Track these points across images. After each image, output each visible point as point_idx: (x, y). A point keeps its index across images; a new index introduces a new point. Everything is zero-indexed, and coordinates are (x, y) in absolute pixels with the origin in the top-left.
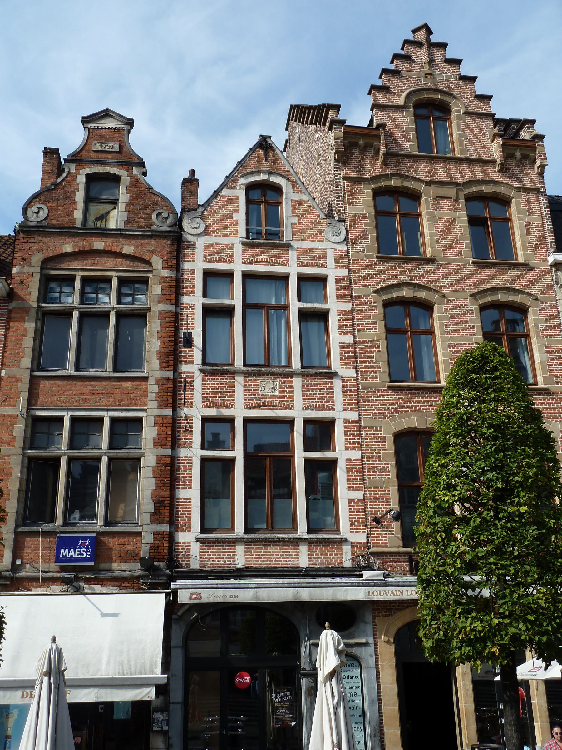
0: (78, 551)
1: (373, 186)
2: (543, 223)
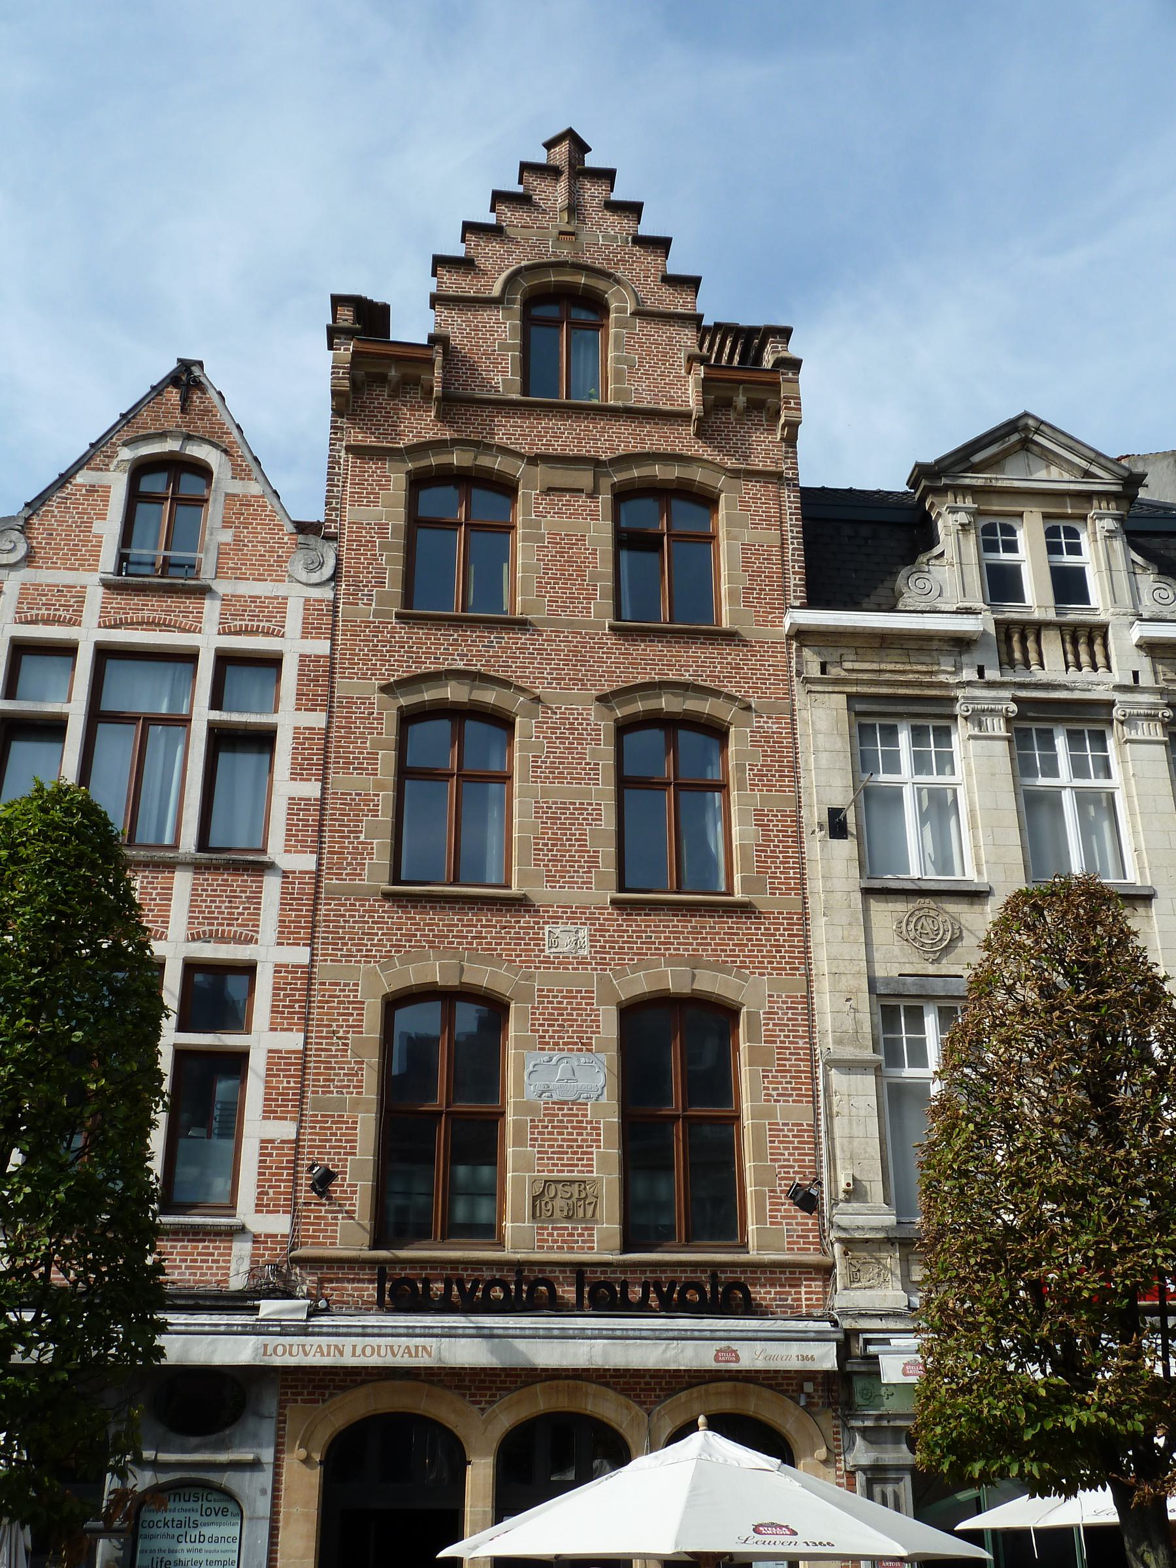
2: (783, 546)
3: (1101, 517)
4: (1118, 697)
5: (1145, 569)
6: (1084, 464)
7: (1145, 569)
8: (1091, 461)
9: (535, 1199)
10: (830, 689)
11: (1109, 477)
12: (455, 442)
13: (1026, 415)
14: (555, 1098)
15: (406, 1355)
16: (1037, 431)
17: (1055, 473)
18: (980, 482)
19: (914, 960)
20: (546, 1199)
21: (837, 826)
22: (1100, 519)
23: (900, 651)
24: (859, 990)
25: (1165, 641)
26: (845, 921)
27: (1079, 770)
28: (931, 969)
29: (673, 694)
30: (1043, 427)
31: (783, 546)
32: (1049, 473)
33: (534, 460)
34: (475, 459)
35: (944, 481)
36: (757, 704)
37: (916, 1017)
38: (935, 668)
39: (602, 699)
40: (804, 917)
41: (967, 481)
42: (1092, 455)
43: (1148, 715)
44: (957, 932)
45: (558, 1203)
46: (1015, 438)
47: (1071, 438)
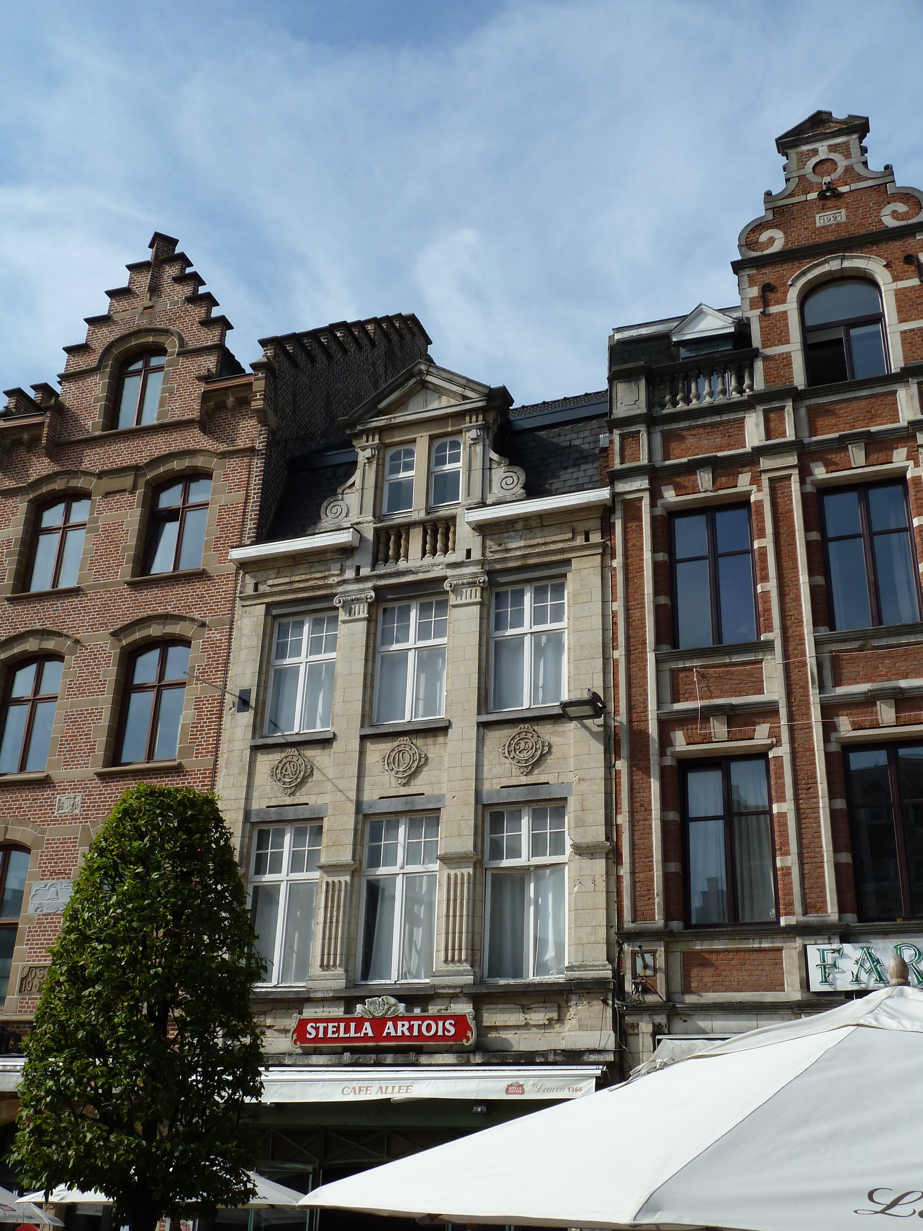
0: (334, 1027)
1: (31, 496)
2: (246, 502)
4: (449, 572)
5: (499, 463)
6: (459, 390)
9: (22, 980)
10: (255, 602)
12: (57, 474)
14: (44, 912)
17: (445, 401)
18: (383, 423)
19: (279, 795)
20: (29, 979)
21: (243, 703)
22: (469, 431)
23: (306, 565)
24: (237, 821)
26: (237, 771)
28: (289, 801)
29: (157, 623)
31: (246, 502)
33: (101, 475)
34: (68, 482)
35: (359, 428)
36: (211, 621)
38: (327, 573)
39: (113, 634)
40: (214, 771)
41: (374, 424)
42: (464, 382)
43: (469, 583)
44: (546, 749)
45: (36, 981)
47: (449, 372)
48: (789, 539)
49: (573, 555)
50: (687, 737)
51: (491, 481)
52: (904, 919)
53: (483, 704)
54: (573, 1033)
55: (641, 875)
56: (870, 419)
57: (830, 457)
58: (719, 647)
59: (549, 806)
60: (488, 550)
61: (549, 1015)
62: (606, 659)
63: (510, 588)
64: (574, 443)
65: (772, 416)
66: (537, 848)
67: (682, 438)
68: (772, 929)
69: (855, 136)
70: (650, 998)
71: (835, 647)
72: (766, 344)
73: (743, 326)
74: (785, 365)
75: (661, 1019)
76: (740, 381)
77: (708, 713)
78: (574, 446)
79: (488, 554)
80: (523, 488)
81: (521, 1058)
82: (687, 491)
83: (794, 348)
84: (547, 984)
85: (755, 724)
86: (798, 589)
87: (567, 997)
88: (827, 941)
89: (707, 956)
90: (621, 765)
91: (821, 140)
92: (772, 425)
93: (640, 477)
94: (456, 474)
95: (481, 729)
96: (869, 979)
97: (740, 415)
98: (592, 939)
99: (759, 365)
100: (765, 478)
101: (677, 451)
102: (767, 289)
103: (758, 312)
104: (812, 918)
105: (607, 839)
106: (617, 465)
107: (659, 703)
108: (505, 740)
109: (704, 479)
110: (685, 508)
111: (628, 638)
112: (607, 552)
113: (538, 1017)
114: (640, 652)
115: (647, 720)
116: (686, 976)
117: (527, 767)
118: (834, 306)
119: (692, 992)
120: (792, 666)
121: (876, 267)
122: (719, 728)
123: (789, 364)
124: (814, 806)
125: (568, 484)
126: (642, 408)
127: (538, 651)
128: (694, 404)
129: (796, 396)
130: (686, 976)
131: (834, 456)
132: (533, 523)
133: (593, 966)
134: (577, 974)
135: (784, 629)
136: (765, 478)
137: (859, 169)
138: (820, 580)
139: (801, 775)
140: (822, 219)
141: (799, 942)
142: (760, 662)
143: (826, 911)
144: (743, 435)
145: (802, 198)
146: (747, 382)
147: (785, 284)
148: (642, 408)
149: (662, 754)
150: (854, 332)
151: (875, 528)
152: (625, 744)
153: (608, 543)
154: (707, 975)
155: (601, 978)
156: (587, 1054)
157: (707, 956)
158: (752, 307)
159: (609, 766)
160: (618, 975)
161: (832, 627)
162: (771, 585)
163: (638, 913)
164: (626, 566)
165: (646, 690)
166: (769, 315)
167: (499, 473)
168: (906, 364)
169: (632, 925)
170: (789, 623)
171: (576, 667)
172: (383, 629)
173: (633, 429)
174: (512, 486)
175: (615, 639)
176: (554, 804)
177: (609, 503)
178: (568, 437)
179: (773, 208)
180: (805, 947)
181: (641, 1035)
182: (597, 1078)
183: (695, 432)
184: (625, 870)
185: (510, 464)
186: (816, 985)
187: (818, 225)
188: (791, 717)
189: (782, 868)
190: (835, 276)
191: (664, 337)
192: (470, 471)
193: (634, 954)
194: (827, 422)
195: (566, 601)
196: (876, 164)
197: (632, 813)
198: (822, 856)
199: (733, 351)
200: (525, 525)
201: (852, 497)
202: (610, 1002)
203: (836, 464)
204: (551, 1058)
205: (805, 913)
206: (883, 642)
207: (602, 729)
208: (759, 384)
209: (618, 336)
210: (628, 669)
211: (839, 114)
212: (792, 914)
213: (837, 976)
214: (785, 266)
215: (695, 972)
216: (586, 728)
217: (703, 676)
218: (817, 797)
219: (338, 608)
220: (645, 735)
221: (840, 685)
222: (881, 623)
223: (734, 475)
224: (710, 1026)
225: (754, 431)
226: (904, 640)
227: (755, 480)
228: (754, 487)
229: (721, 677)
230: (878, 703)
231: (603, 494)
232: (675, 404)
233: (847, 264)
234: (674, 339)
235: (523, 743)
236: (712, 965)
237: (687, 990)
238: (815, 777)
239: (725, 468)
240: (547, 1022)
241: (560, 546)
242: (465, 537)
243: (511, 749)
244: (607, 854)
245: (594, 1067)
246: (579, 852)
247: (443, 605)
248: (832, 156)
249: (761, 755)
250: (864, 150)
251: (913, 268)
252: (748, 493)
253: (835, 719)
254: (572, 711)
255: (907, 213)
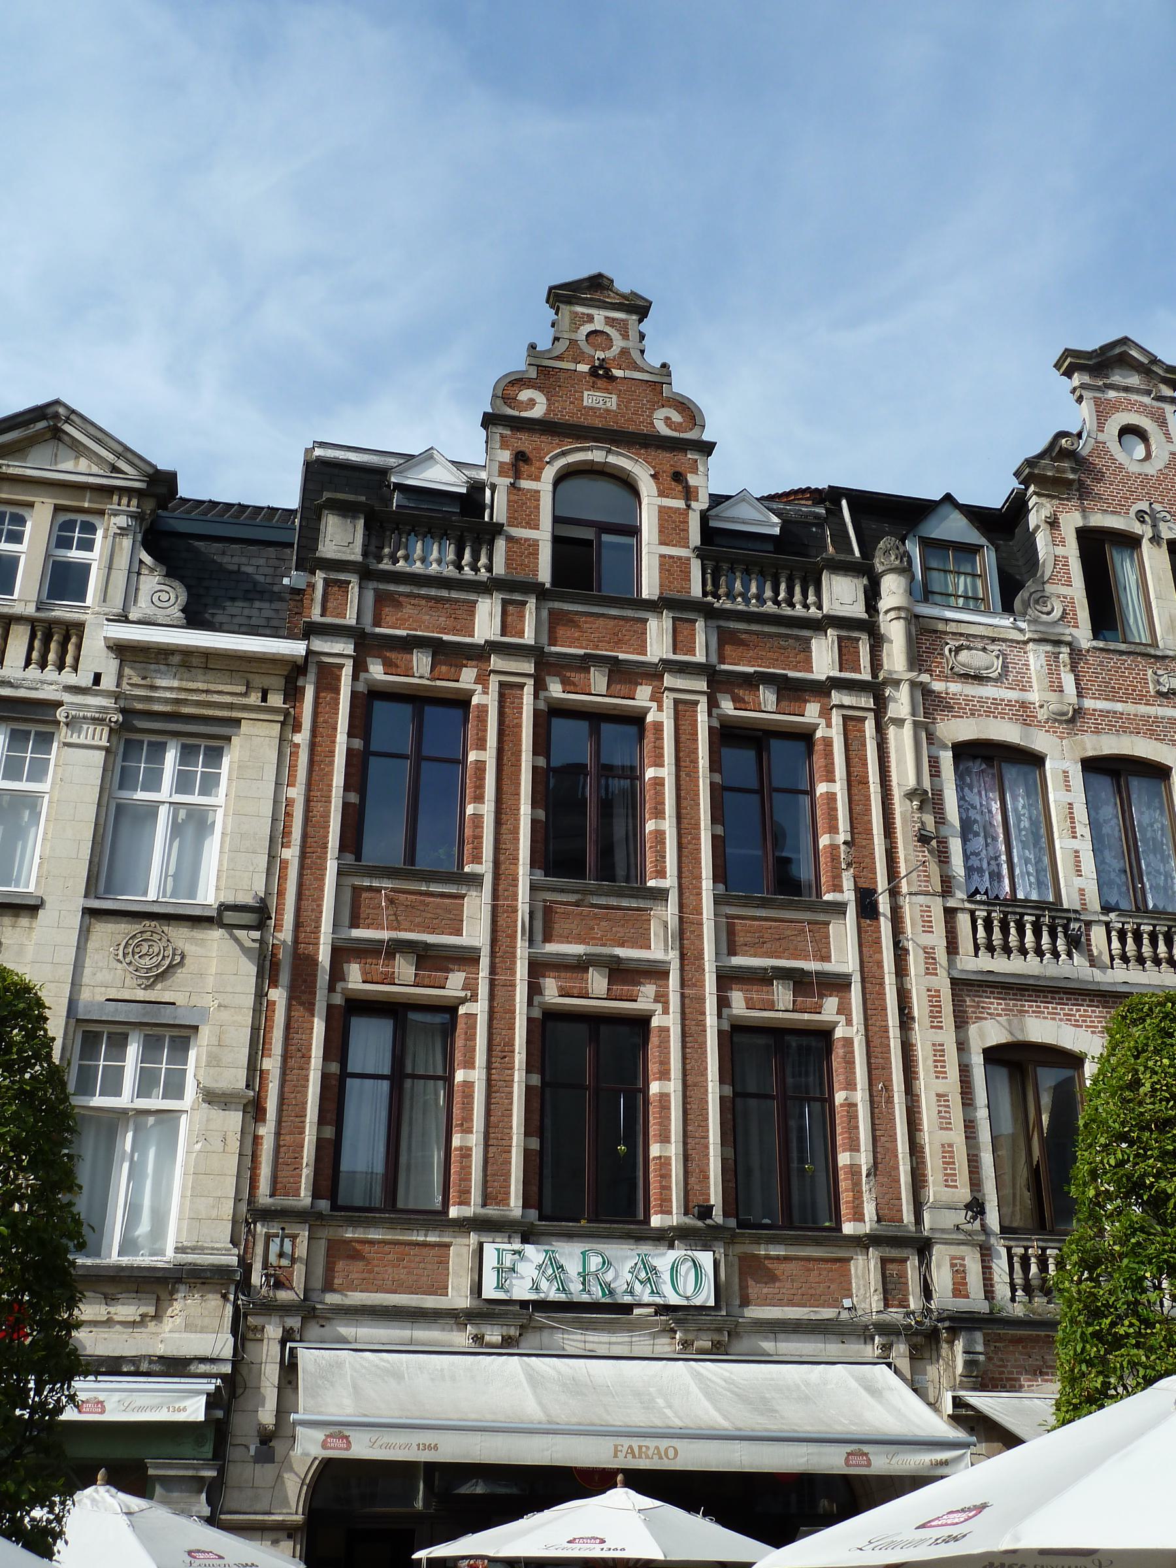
3: (116, 514)
4: (67, 698)
5: (152, 570)
6: (111, 457)
7: (152, 570)
8: (119, 456)
11: (135, 473)
13: (57, 402)
15: (630, 1456)
16: (68, 420)
17: (83, 465)
22: (115, 515)
25: (136, 644)
27: (183, 783)
30: (73, 417)
32: (77, 464)
37: (119, 1043)
42: (120, 449)
43: (94, 719)
44: (178, 959)
46: (41, 425)
47: (101, 430)
48: (513, 758)
49: (245, 715)
50: (364, 973)
51: (137, 589)
52: (589, 1221)
53: (92, 887)
54: (176, 1335)
55: (287, 1138)
56: (616, 643)
57: (568, 674)
58: (409, 869)
59: (168, 1033)
60: (125, 681)
61: (143, 1310)
62: (272, 857)
63: (147, 738)
64: (244, 569)
65: (510, 608)
66: (145, 1086)
67: (398, 605)
68: (437, 1219)
69: (634, 317)
70: (283, 1295)
71: (550, 896)
72: (513, 521)
73: (477, 488)
74: (530, 554)
75: (294, 1322)
76: (476, 557)
77: (396, 948)
78: (244, 573)
79: (125, 686)
80: (182, 611)
81: (101, 1365)
82: (399, 671)
83: (543, 535)
84: (139, 1268)
85: (448, 970)
86: (518, 820)
87: (173, 1287)
88: (506, 1240)
89: (358, 1246)
90: (278, 995)
91: (599, 307)
92: (509, 619)
93: (344, 639)
94: (86, 568)
95: (87, 917)
96: (550, 1288)
97: (472, 597)
98: (214, 1214)
99: (500, 544)
100: (494, 681)
101: (390, 619)
102: (521, 458)
103: (508, 481)
104: (491, 1211)
105: (247, 1086)
106: (316, 615)
107: (336, 925)
108: (119, 937)
109: (421, 662)
110: (389, 690)
111: (305, 836)
112: (291, 723)
113: (126, 1311)
114: (320, 858)
115: (318, 944)
116: (330, 1270)
117: (148, 978)
118: (595, 501)
119: (333, 1291)
120: (500, 910)
121: (642, 473)
122: (405, 968)
123: (535, 554)
124: (507, 1078)
125: (237, 620)
126: (355, 554)
127: (176, 829)
128: (418, 567)
129: (541, 593)
130: (330, 1270)
131: (573, 675)
132: (195, 661)
133: (213, 1248)
134: (190, 1258)
135: (497, 863)
136: (494, 681)
137: (635, 355)
138: (354, 798)
139: (497, 1039)
140: (592, 398)
141: (473, 1238)
142: (463, 897)
143: (508, 1205)
144: (473, 621)
145: (571, 366)
146: (483, 560)
147: (541, 459)
148: (355, 554)
149: (331, 989)
150: (606, 538)
151: (425, 753)
152: (285, 969)
153: (291, 710)
154: (356, 1269)
155: (222, 1266)
156: (196, 1362)
157: (358, 1246)
158: (501, 473)
159: (260, 995)
160: (245, 1266)
161: (358, 858)
162: (487, 809)
163: (279, 1186)
164: (313, 746)
165: (320, 906)
166: (519, 489)
167: (150, 583)
168: (661, 593)
169: (269, 1201)
170: (502, 857)
171: (231, 860)
172: (123, 767)
173: (342, 577)
174: (166, 605)
175: (286, 833)
176: (176, 1032)
177: (301, 661)
178: (236, 560)
179: (538, 366)
180: (481, 1245)
181: (265, 1341)
182: (208, 1395)
183: (416, 602)
184: (267, 1131)
185: (167, 575)
186: (490, 1291)
187: (585, 404)
188: (493, 970)
189: (461, 1148)
190: (595, 468)
191: (382, 473)
192: (110, 568)
193: (268, 1238)
194: (569, 634)
195: (53, 756)
196: (653, 359)
197: (285, 1057)
198: (511, 1138)
199: (461, 516)
200: (183, 660)
201: (407, 710)
202: (232, 1297)
203: (574, 684)
204: (144, 1367)
205: (484, 1205)
206: (602, 901)
207: (257, 945)
208: (499, 569)
209: (318, 452)
210: (301, 875)
211: (623, 285)
212: (468, 1204)
213: (514, 1282)
214: (543, 438)
215: (340, 1265)
216: (236, 940)
217: (391, 901)
218: (513, 1068)
219: (59, 722)
220: (313, 962)
221: (550, 942)
222: (413, 864)
223: (456, 666)
224: (353, 1333)
225: (486, 621)
226: (625, 903)
227: (482, 679)
228: (479, 688)
229: (413, 907)
230: (591, 969)
231: (296, 648)
232: (395, 561)
233: (612, 459)
234: (393, 479)
235: (145, 946)
236: (363, 1258)
237: (329, 1287)
238: (513, 1045)
239: (449, 655)
240: (138, 1319)
241: (228, 699)
242: (95, 655)
243: (131, 949)
244: (245, 1106)
245: (205, 1381)
246: (209, 1099)
247: (45, 740)
248: (608, 330)
249: (450, 1009)
250: (642, 337)
251: (680, 488)
252: (471, 693)
253: (541, 980)
254: (230, 917)
255: (681, 424)
